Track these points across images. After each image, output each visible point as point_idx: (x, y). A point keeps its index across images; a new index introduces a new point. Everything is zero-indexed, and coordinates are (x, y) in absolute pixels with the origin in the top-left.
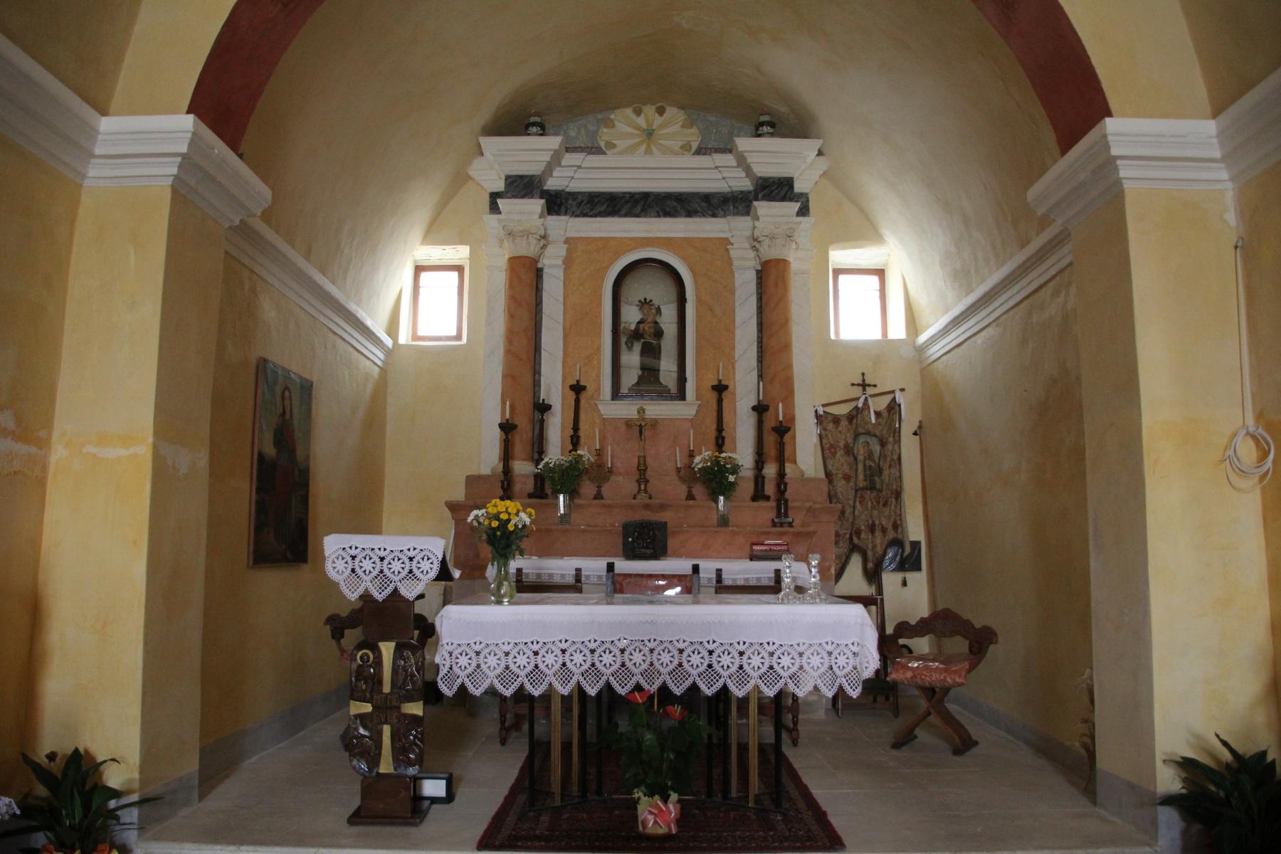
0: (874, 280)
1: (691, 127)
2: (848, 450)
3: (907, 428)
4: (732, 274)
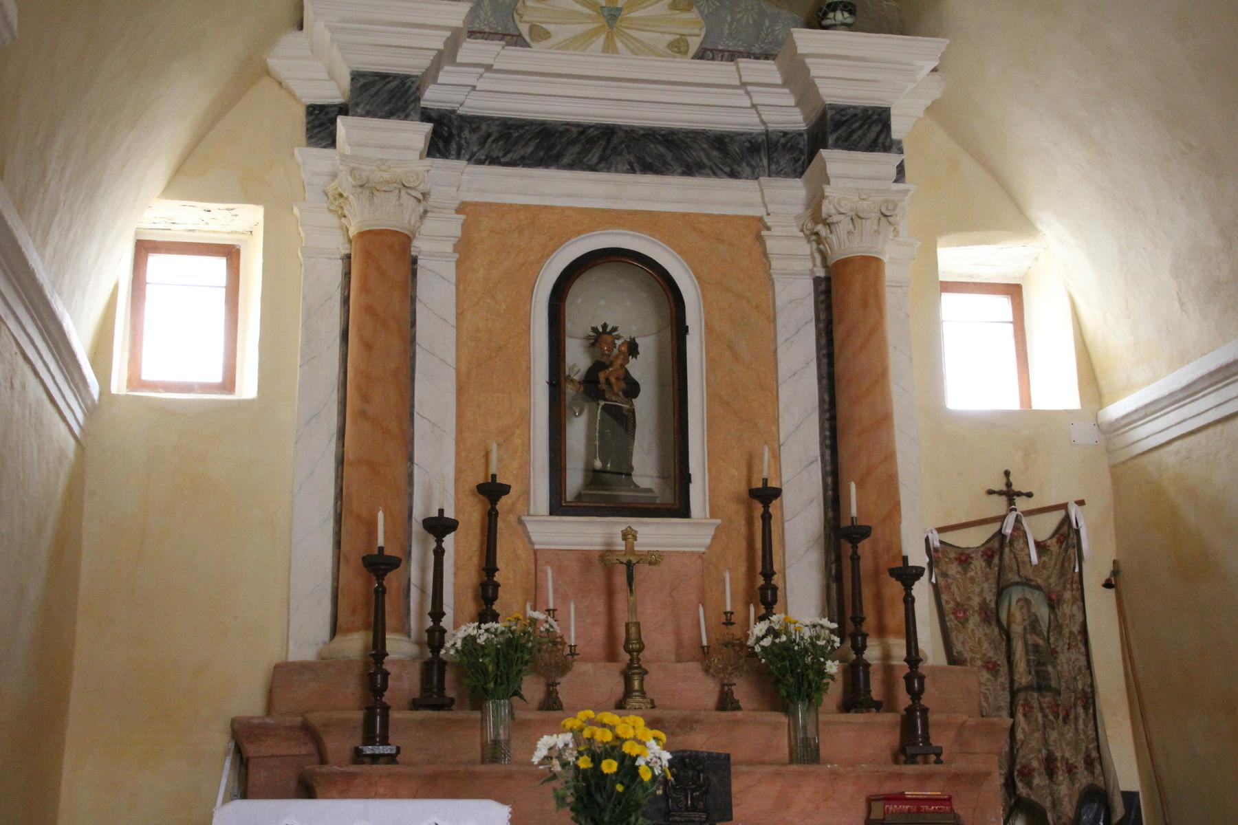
1: (688, 9)
2: (990, 615)
3: (1095, 570)
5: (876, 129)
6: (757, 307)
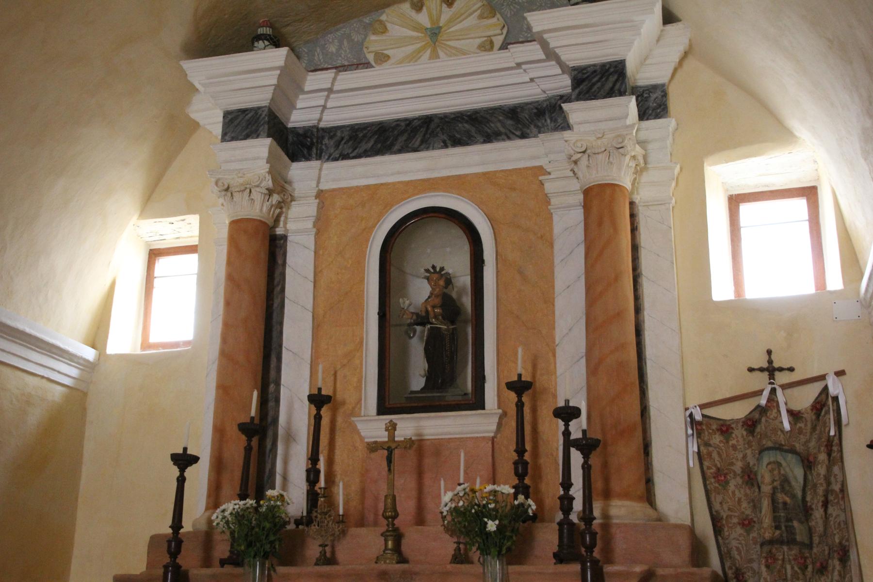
0: (801, 205)
5: (613, 79)
6: (542, 237)
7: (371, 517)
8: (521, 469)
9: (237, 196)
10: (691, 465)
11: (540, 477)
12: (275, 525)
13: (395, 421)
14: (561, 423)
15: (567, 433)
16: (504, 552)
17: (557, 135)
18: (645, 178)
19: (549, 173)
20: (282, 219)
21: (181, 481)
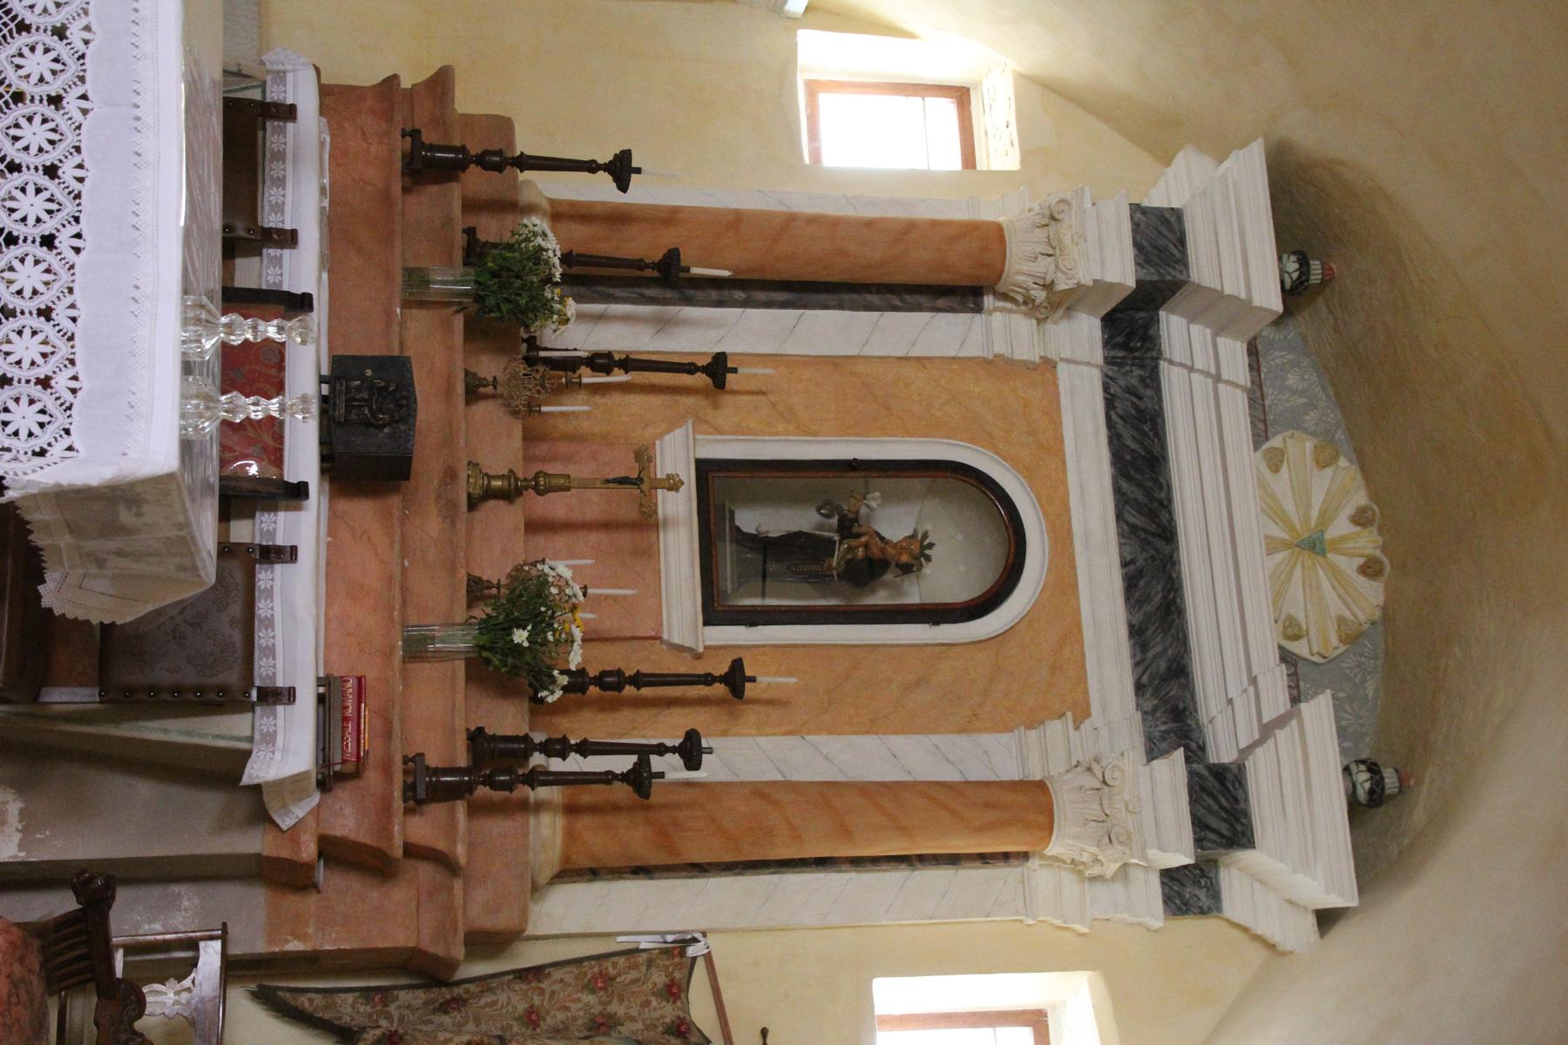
4: (1007, 728)
5: (1223, 828)
7: (541, 449)
8: (612, 681)
9: (1041, 234)
10: (620, 939)
11: (602, 709)
12: (523, 312)
13: (683, 489)
14: (677, 742)
15: (661, 750)
16: (484, 654)
17: (1139, 741)
18: (1067, 878)
19: (1077, 728)
20: (1009, 305)
21: (591, 167)
